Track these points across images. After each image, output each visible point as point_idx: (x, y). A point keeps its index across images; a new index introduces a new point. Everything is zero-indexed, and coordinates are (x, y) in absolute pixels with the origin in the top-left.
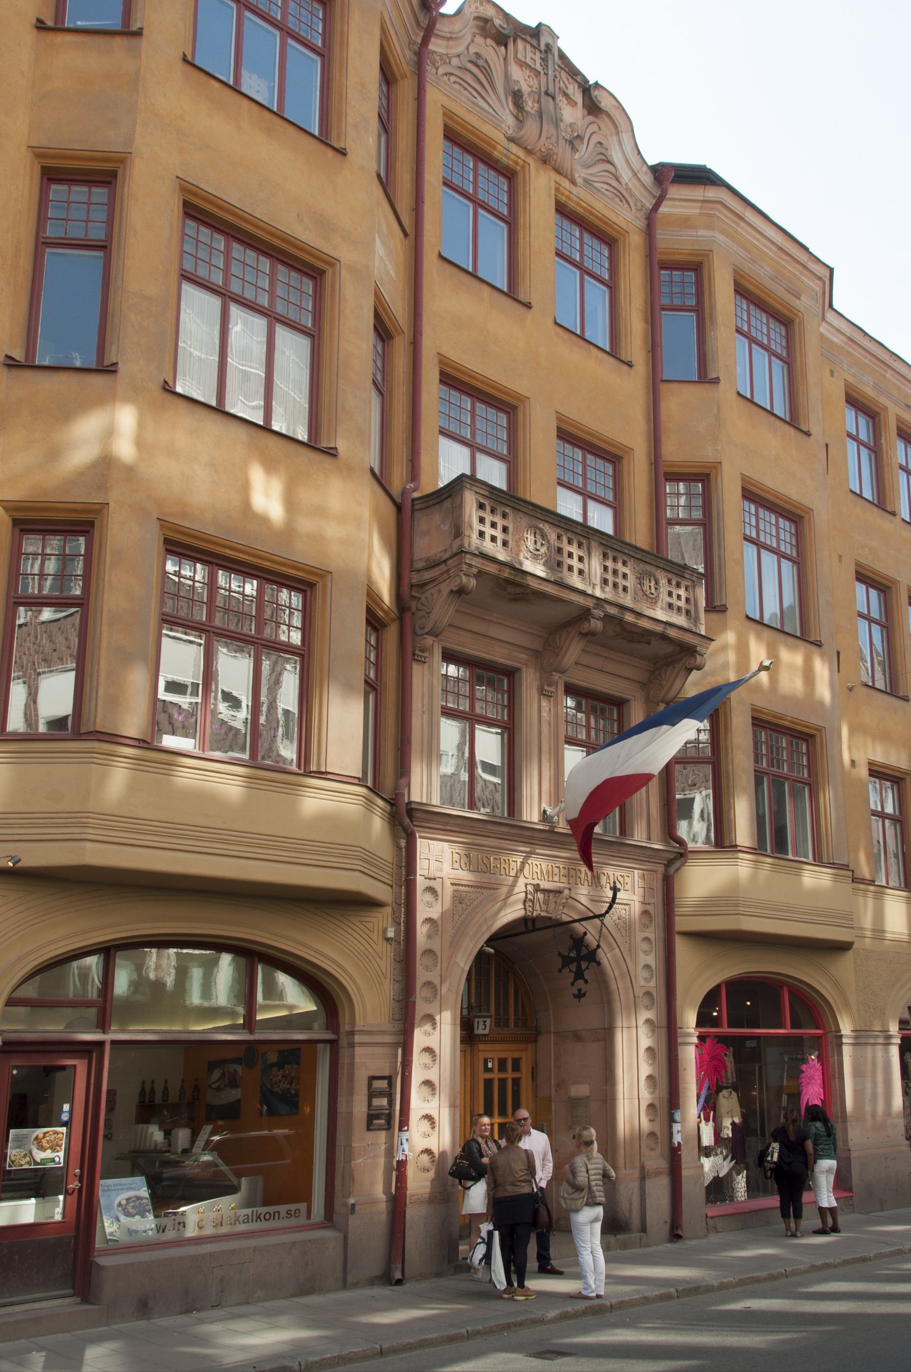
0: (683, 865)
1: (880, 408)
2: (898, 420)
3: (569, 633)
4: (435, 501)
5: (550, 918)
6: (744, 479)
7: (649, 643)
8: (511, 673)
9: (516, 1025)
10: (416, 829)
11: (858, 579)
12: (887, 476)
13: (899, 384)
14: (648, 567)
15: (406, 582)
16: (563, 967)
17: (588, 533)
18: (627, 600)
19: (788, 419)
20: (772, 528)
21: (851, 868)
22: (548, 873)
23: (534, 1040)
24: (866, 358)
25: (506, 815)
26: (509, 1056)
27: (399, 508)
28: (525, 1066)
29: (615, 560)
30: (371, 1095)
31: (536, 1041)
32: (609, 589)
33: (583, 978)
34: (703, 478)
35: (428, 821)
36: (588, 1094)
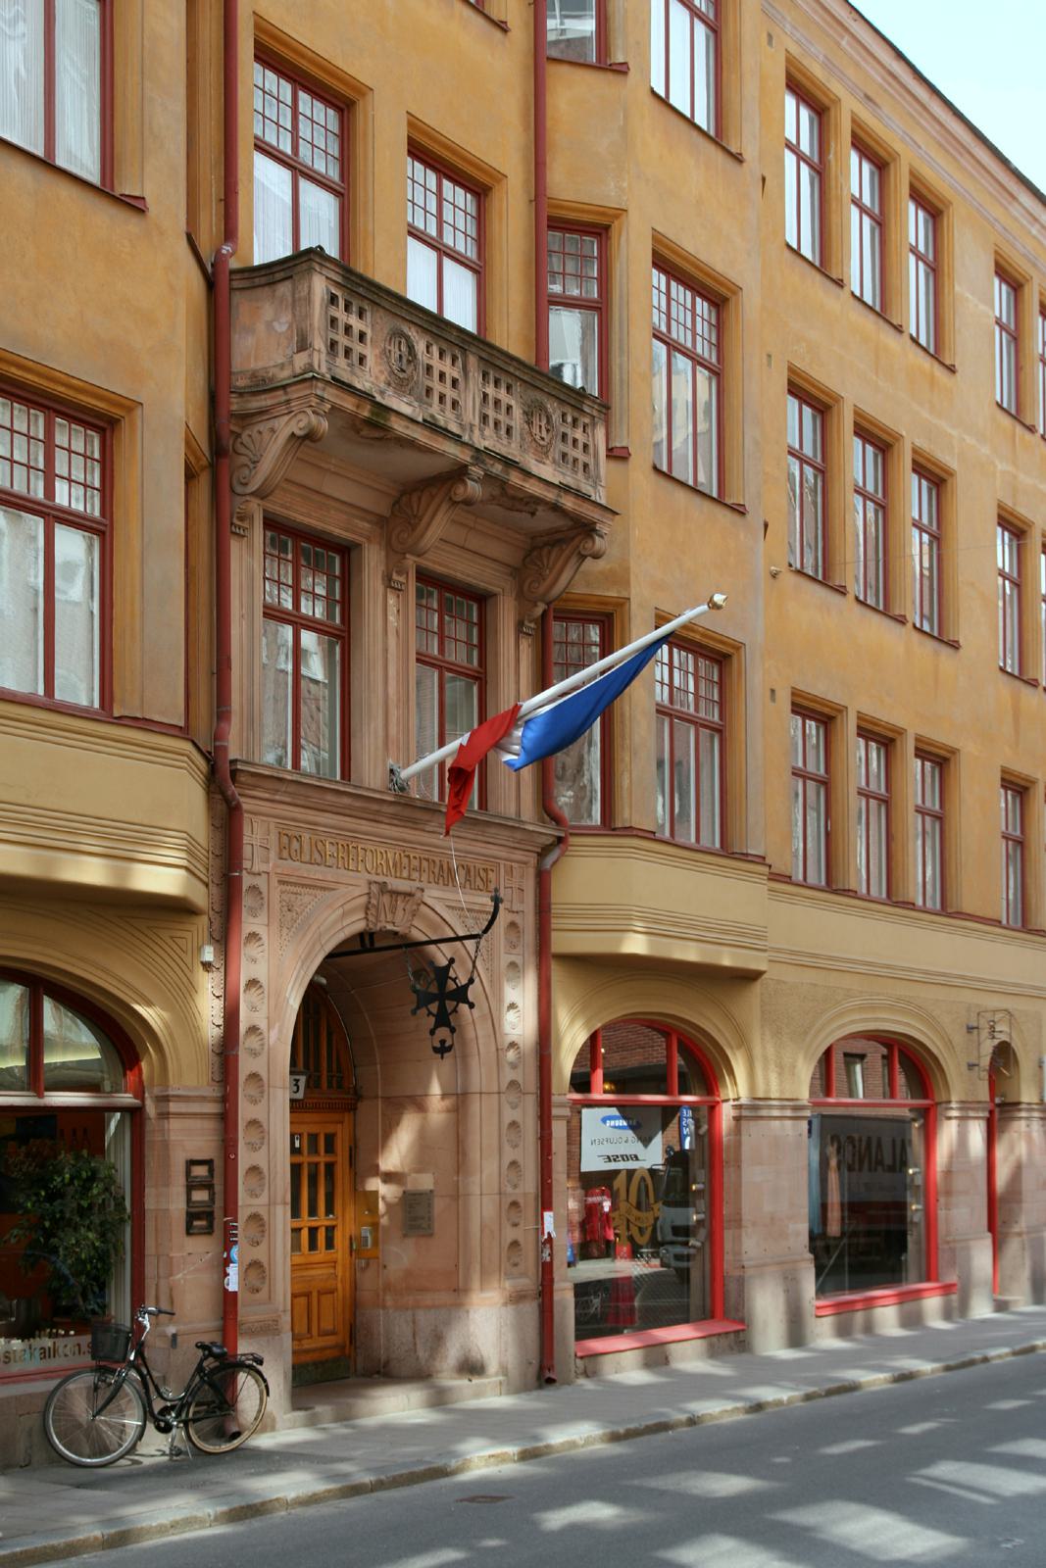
0: (563, 854)
1: (831, 100)
2: (854, 121)
3: (433, 497)
4: (263, 280)
5: (396, 933)
6: (657, 238)
7: (533, 514)
8: (346, 551)
9: (330, 1086)
10: (242, 799)
11: (791, 392)
12: (834, 218)
13: (858, 58)
14: (538, 396)
15: (223, 412)
16: (418, 1008)
17: (464, 341)
18: (512, 450)
19: (712, 133)
20: (690, 317)
21: (768, 861)
22: (395, 865)
23: (351, 1108)
24: (816, 12)
25: (338, 778)
26: (322, 1131)
27: (211, 283)
28: (342, 1146)
29: (497, 383)
30: (191, 1186)
31: (355, 1109)
32: (489, 431)
33: (447, 1024)
34: (595, 229)
35: (254, 787)
36: (431, 1187)
